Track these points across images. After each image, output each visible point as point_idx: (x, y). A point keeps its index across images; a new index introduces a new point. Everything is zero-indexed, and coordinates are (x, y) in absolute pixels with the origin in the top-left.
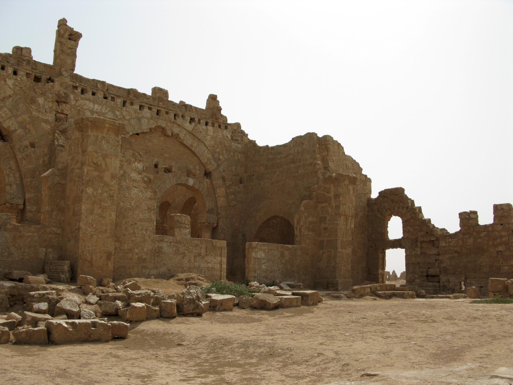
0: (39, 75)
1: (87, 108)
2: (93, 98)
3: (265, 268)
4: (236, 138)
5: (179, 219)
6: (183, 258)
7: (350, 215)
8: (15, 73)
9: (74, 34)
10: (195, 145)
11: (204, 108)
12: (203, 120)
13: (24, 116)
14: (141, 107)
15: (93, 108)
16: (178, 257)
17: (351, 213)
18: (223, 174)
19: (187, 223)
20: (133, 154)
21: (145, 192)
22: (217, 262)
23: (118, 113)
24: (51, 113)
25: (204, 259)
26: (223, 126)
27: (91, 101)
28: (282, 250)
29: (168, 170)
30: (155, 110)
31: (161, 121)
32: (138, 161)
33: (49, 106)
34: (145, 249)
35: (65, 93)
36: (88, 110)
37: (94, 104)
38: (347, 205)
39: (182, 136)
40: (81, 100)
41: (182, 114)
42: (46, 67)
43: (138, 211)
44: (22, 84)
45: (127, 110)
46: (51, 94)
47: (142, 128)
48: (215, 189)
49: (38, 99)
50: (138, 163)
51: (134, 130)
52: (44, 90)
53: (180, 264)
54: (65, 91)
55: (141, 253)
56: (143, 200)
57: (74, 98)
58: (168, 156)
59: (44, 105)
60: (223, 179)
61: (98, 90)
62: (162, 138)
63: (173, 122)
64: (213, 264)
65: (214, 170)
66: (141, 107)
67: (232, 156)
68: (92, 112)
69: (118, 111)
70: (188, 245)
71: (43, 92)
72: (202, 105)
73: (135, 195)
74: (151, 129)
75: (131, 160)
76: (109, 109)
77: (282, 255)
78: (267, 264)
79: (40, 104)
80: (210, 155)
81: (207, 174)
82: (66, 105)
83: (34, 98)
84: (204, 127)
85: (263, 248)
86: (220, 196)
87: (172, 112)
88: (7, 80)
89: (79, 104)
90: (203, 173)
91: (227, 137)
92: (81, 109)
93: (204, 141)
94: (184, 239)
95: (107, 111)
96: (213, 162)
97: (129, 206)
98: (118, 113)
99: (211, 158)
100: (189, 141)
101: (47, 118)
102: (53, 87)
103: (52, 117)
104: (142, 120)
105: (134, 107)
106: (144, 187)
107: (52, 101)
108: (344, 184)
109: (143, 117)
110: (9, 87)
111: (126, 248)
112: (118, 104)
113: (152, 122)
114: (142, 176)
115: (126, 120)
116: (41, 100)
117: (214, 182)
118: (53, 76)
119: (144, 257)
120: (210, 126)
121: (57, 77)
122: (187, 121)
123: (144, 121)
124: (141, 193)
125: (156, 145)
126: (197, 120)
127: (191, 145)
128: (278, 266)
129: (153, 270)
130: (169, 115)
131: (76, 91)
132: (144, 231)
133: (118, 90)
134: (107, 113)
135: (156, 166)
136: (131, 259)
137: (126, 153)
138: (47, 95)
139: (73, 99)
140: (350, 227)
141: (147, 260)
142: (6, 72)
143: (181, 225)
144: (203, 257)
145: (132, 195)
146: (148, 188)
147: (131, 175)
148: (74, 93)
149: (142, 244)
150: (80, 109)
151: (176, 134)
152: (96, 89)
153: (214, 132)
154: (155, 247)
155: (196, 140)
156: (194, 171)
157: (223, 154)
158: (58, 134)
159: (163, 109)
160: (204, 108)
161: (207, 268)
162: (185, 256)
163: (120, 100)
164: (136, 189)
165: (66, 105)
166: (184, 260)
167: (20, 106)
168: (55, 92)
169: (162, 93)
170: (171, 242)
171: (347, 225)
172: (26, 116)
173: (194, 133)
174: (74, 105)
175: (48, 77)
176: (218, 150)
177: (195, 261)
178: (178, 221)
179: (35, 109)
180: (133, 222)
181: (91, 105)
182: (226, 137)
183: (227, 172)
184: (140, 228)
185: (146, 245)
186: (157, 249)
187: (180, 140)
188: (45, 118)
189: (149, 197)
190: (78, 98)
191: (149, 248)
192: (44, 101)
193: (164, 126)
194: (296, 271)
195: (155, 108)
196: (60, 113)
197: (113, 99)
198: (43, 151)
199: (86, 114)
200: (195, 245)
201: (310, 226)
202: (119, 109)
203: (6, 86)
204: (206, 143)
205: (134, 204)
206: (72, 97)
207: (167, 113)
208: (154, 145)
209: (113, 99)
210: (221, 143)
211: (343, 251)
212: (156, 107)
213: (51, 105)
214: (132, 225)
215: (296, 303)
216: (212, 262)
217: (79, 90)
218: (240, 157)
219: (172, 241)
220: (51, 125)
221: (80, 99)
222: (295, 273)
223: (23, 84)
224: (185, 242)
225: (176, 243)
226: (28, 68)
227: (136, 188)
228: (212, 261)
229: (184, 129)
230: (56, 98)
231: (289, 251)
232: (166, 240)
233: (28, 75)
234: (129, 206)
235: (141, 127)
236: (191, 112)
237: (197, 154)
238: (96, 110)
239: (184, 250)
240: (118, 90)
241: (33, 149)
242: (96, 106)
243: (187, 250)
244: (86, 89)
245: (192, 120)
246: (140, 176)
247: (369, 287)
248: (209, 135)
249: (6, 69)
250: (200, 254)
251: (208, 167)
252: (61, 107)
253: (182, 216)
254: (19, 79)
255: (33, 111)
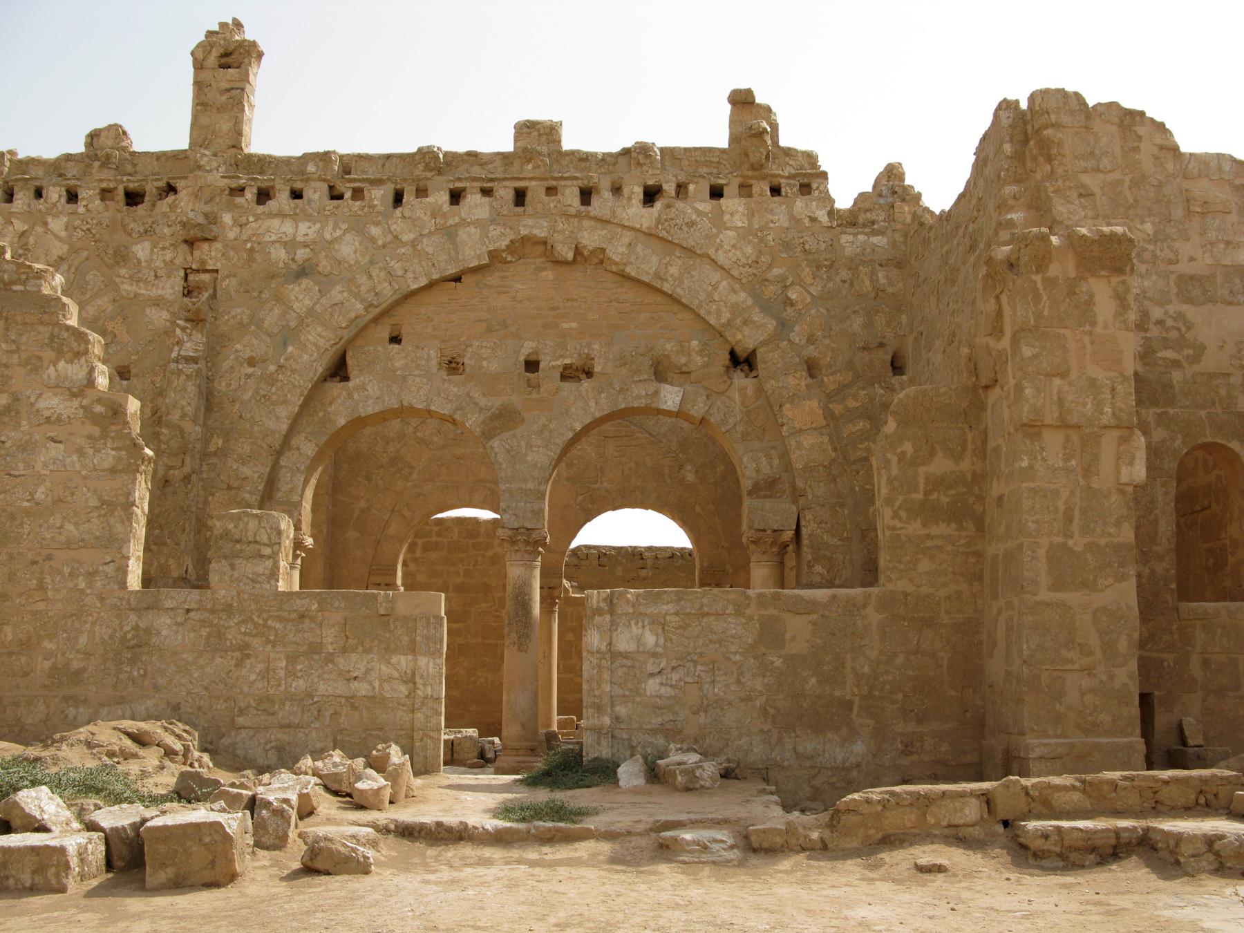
0: (136, 185)
1: (274, 238)
2: (292, 205)
3: (667, 691)
4: (868, 215)
5: (231, 526)
6: (239, 664)
7: (1107, 418)
8: (72, 197)
9: (234, 50)
10: (673, 270)
11: (724, 144)
12: (696, 183)
13: (99, 302)
14: (456, 197)
15: (294, 235)
16: (218, 660)
17: (1108, 410)
18: (811, 351)
19: (265, 540)
20: (52, 336)
21: (91, 452)
22: (396, 674)
23: (375, 231)
24: (169, 277)
25: (331, 666)
26: (791, 186)
27: (285, 216)
28: (771, 611)
29: (576, 373)
30: (505, 193)
31: (530, 222)
32: (69, 355)
33: (164, 261)
34: (83, 640)
35: (206, 215)
36: (277, 245)
37: (296, 222)
38: (1074, 374)
39: (617, 251)
40: (256, 221)
41: (613, 183)
42: (163, 159)
43: (59, 516)
44: (90, 221)
45: (407, 215)
46: (169, 226)
47: (460, 257)
48: (776, 408)
49: (134, 249)
50: (71, 362)
51: (433, 270)
52: (150, 221)
53: (226, 684)
54: (207, 209)
55: (63, 654)
56: (85, 478)
57: (235, 221)
58: (574, 325)
59: (152, 260)
60: (812, 368)
61: (308, 180)
62: (549, 275)
63: (575, 216)
64: (377, 684)
65: (765, 343)
66: (456, 197)
67: (844, 282)
68: (290, 245)
69: (377, 224)
70: (265, 616)
71: (147, 226)
72: (718, 137)
73: (51, 467)
74: (493, 255)
75: (40, 358)
76: (344, 226)
77: (771, 634)
78: (675, 676)
79: (139, 261)
80: (743, 295)
81: (742, 361)
82: (210, 246)
83: (122, 249)
84: (706, 206)
85: (652, 610)
86: (801, 431)
87: (569, 183)
88: (49, 219)
89: (250, 232)
90: (725, 358)
91: (813, 219)
92: (255, 245)
93: (711, 252)
94: (246, 597)
95: (338, 233)
96: (757, 316)
97: (26, 504)
98: (375, 231)
99: (750, 302)
100: (646, 263)
101: (160, 292)
102: (173, 207)
103: (173, 288)
104: (460, 233)
105: (428, 199)
106: (90, 437)
107: (172, 245)
108: (1046, 280)
109: (464, 223)
110: (56, 236)
111: (10, 636)
112: (376, 202)
113: (495, 231)
114: (85, 402)
115: (404, 244)
116: (142, 250)
117: (769, 386)
118: (173, 178)
119: (75, 665)
120: (732, 198)
121: (186, 178)
122: (630, 199)
123: (470, 236)
124: (75, 458)
125: (528, 299)
126: (669, 188)
127: (657, 276)
128: (739, 682)
129: (106, 709)
130: (559, 197)
131: (239, 200)
132: (81, 578)
133: (383, 165)
134: (340, 237)
135: (532, 365)
136: (26, 674)
137: (24, 339)
138: (157, 231)
139: (230, 223)
140: (1118, 479)
141: (86, 675)
142: (46, 202)
143: (238, 546)
144: (330, 659)
145: (39, 466)
146: (105, 435)
147: (41, 405)
148: (231, 207)
149: (70, 623)
150: (252, 247)
151: (593, 252)
152: (302, 181)
153: (751, 214)
154: (121, 628)
155: (677, 253)
156: (683, 360)
157: (800, 282)
158: (183, 329)
159: (534, 183)
160: (724, 144)
161: (346, 698)
162: (248, 656)
163: (382, 192)
164: (57, 445)
165: (210, 246)
166: (244, 672)
167: (89, 277)
168: (179, 219)
169: (536, 134)
170: (188, 611)
171: (1088, 471)
172: (106, 299)
173: (663, 234)
174: (236, 239)
175: (162, 184)
176: (776, 271)
177: (291, 673)
178: (226, 535)
179: (127, 276)
180: (40, 553)
181: (288, 228)
182: (806, 221)
183: (827, 341)
184: (66, 570)
185: (88, 626)
186: (129, 636)
187: (614, 268)
188: (154, 293)
189: (107, 464)
190: (244, 218)
191: (97, 636)
192: (152, 250)
193: (540, 233)
194: (857, 699)
195: (505, 187)
196: (198, 271)
197: (358, 194)
198: (153, 383)
199: (273, 256)
200: (294, 615)
201: (935, 496)
202: (380, 218)
203: (50, 236)
204: (721, 257)
205: (47, 495)
206: (227, 218)
207: (551, 191)
208: (520, 302)
209: (358, 194)
210: (787, 246)
211: (1073, 598)
212: (507, 183)
213: (169, 255)
214: (34, 563)
215: (34, 872)
216: (373, 675)
217: (250, 195)
218: (882, 280)
219: (193, 606)
220: (170, 309)
221: (251, 219)
222: (851, 710)
223: (92, 219)
224: (253, 607)
225: (212, 611)
226: (106, 174)
227: (55, 442)
228: (368, 671)
229: (624, 227)
230: (182, 234)
231: (815, 616)
232: (169, 604)
233: (106, 194)
234: (26, 504)
235: (457, 253)
236: (645, 168)
237: (683, 300)
238: (302, 239)
239: (245, 634)
240: (383, 165)
241: (125, 382)
242: (303, 227)
243: (255, 636)
244: (273, 187)
245: (651, 195)
246: (76, 403)
247: (972, 794)
248: (727, 229)
249: (44, 195)
250: (315, 649)
251: (739, 336)
252: (197, 253)
253: (247, 514)
254: (81, 210)
255: (122, 283)
